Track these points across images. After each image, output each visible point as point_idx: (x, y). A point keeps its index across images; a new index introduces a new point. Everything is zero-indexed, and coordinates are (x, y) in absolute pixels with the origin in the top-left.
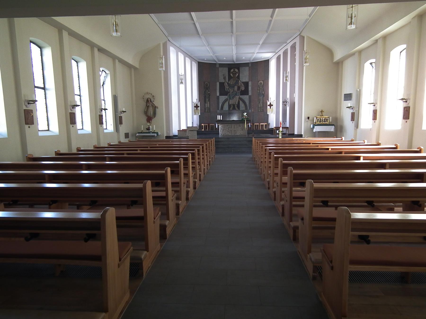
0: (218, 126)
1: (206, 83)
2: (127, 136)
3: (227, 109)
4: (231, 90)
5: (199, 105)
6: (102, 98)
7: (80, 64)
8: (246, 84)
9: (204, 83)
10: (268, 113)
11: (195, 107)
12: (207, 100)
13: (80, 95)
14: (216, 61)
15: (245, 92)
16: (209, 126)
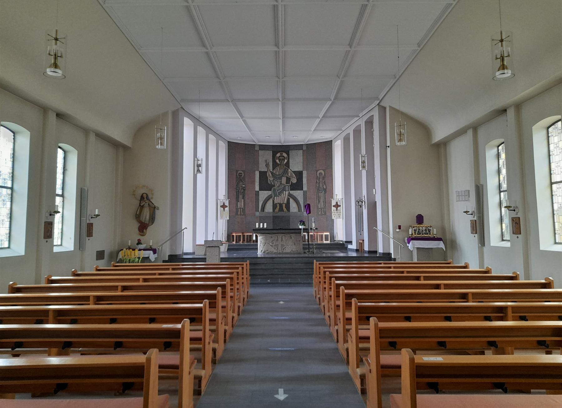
0: (256, 237)
2: (100, 255)
3: (271, 210)
4: (277, 184)
5: (227, 204)
6: (59, 191)
7: (19, 139)
8: (299, 175)
9: (237, 171)
10: (333, 218)
11: (221, 206)
12: (241, 196)
13: (12, 189)
14: (254, 142)
15: (298, 186)
16: (244, 236)
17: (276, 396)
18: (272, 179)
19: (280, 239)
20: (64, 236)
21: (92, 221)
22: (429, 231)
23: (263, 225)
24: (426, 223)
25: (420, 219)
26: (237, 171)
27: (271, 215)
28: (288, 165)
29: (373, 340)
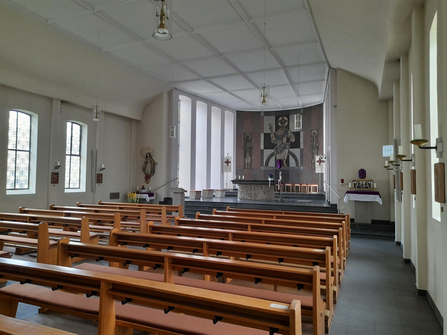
1: (246, 135)
4: (279, 143)
8: (297, 134)
9: (245, 134)
12: (248, 154)
13: (30, 151)
15: (296, 145)
17: (40, 308)
18: (274, 139)
19: (253, 189)
21: (101, 172)
22: (369, 185)
23: (241, 177)
24: (369, 176)
25: (362, 174)
26: (245, 134)
27: (274, 169)
28: (288, 127)
29: (318, 282)
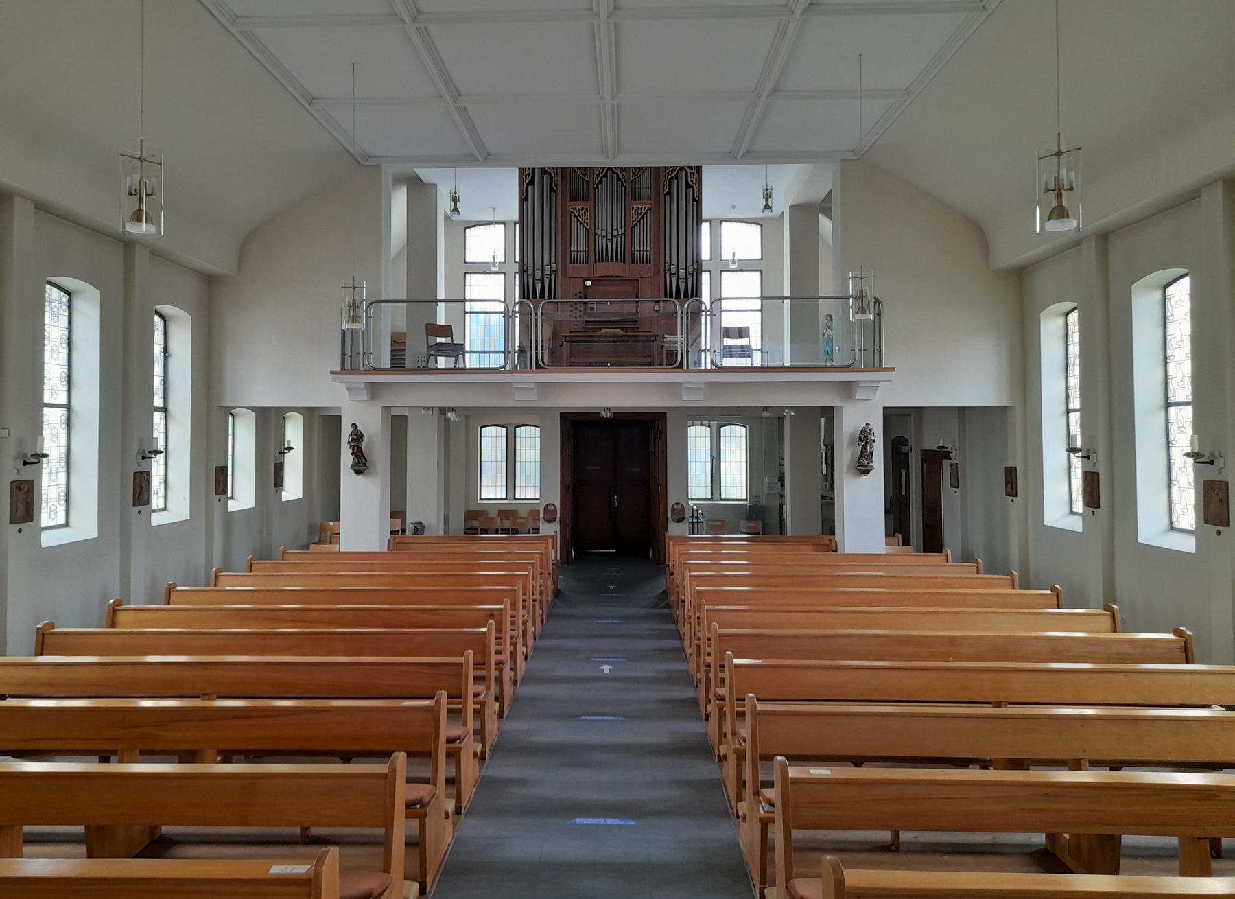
6: (158, 402)
7: (77, 303)
13: (68, 407)
20: (172, 495)
